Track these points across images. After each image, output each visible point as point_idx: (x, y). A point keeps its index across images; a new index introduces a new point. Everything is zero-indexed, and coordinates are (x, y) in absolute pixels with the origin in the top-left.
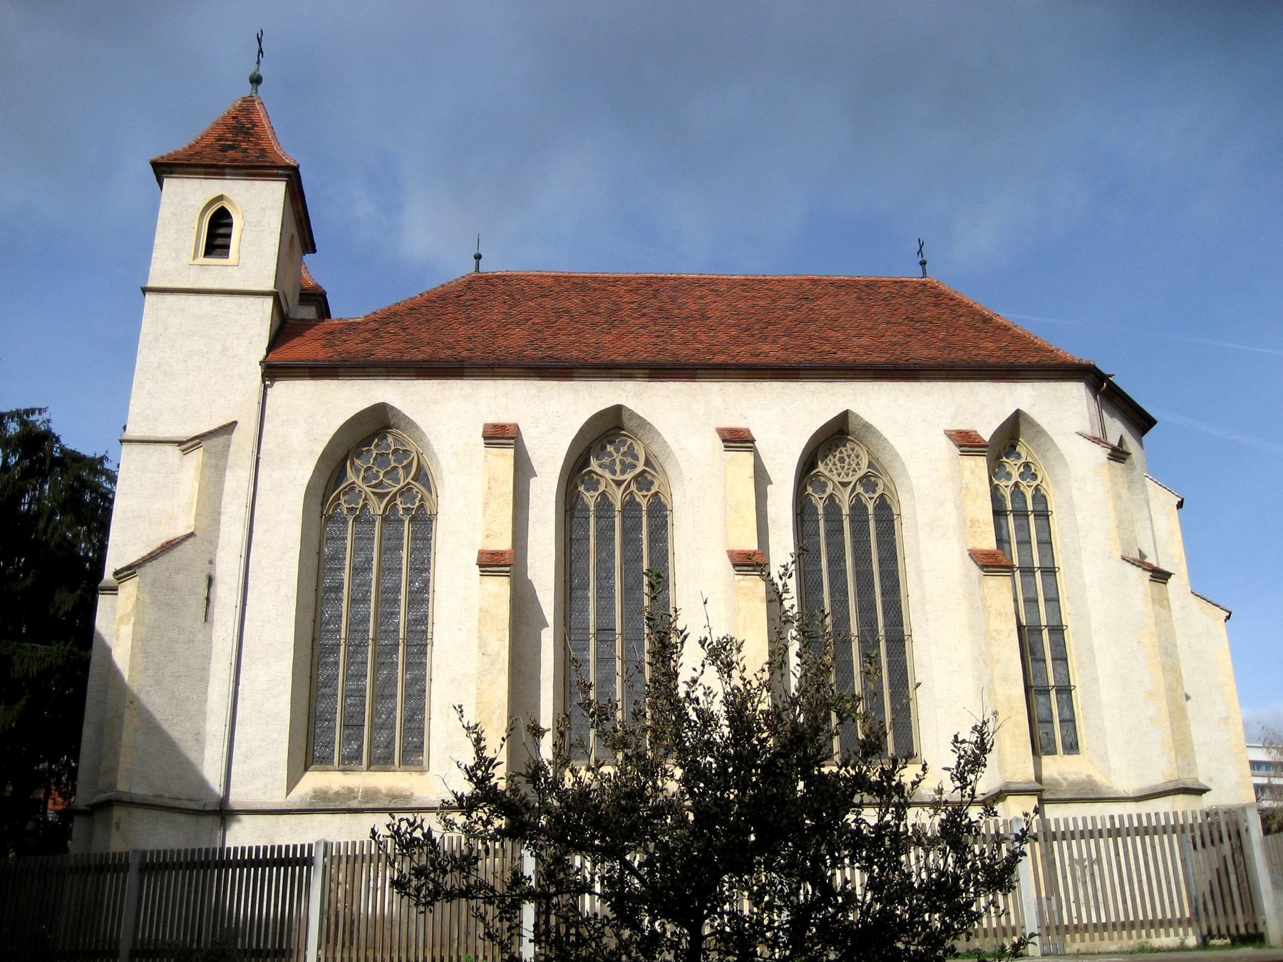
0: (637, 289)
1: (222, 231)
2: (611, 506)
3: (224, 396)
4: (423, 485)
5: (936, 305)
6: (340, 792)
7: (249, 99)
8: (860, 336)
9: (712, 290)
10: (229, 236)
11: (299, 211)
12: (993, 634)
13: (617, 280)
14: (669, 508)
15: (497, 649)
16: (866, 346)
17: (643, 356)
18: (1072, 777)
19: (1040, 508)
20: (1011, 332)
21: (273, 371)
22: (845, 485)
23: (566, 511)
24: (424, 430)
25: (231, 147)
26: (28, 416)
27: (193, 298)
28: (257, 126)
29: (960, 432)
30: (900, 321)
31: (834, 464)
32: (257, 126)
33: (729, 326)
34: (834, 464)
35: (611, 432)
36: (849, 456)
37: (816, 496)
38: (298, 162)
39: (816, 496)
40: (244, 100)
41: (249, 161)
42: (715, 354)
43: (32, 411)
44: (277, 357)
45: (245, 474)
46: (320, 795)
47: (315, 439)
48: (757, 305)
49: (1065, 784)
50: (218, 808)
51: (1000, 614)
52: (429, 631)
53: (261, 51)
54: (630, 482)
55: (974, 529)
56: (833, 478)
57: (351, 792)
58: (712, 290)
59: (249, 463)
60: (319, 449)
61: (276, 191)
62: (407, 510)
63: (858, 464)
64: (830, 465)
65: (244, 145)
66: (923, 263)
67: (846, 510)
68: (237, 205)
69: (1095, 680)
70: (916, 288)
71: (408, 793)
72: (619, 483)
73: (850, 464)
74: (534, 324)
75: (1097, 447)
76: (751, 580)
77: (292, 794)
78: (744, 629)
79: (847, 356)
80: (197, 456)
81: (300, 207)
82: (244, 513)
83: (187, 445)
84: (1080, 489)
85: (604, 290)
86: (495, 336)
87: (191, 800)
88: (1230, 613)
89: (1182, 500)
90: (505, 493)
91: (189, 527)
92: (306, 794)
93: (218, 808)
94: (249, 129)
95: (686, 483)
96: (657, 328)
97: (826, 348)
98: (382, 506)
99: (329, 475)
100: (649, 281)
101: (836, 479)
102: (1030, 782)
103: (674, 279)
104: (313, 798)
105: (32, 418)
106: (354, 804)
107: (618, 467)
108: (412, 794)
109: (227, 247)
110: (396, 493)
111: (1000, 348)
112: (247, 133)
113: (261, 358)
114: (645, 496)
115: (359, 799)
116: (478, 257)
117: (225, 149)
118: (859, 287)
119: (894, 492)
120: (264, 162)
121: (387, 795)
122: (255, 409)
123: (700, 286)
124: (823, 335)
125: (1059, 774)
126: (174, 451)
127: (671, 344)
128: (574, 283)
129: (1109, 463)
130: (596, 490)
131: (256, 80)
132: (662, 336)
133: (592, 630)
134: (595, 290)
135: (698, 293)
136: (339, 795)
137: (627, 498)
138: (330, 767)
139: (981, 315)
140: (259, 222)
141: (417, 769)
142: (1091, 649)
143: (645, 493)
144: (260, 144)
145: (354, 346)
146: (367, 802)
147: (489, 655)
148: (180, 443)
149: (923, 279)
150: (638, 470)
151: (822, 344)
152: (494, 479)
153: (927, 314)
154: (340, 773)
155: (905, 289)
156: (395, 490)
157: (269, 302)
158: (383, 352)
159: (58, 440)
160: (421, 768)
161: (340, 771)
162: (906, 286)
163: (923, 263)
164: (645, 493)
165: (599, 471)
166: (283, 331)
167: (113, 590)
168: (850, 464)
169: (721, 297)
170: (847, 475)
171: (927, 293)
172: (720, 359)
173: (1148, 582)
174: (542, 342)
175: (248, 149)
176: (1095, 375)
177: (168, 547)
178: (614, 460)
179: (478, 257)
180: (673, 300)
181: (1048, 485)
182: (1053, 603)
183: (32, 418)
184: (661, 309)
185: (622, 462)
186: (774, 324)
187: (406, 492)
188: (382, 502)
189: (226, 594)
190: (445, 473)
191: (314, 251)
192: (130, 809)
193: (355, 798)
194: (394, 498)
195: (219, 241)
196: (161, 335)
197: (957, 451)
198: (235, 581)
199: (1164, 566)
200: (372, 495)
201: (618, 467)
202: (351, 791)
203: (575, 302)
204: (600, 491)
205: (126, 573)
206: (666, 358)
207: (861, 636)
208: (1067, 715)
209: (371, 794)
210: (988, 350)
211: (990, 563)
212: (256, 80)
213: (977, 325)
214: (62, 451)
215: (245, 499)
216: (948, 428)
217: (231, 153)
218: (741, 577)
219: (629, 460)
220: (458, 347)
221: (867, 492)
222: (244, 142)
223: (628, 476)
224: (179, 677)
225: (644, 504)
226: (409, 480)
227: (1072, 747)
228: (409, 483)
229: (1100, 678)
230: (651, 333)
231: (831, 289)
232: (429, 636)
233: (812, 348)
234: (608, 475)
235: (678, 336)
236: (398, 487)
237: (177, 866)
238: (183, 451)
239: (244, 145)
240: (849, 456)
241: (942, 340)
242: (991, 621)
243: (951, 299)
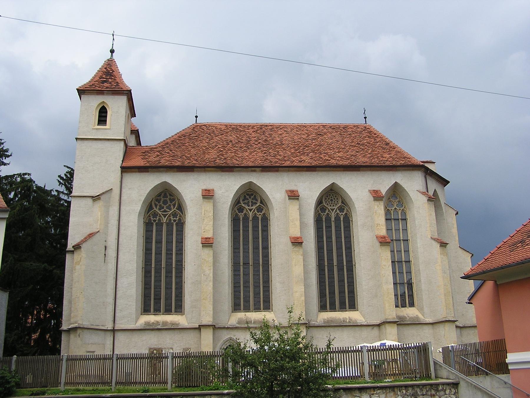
0: (257, 130)
1: (103, 115)
2: (248, 218)
3: (108, 179)
4: (180, 211)
5: (369, 137)
6: (155, 322)
7: (110, 60)
8: (339, 152)
9: (285, 131)
10: (106, 117)
11: (130, 104)
12: (383, 266)
13: (249, 126)
14: (269, 219)
15: (209, 273)
16: (341, 157)
17: (259, 163)
18: (411, 316)
19: (404, 218)
20: (396, 149)
21: (124, 169)
22: (333, 210)
23: (232, 220)
24: (180, 192)
25: (105, 81)
26: (24, 176)
27: (94, 142)
28: (114, 72)
29: (374, 191)
30: (355, 145)
31: (329, 202)
32: (114, 72)
33: (291, 148)
34: (329, 202)
35: (248, 190)
36: (334, 199)
37: (322, 214)
38: (131, 88)
39: (322, 214)
40: (108, 60)
41: (112, 88)
42: (285, 161)
43: (25, 174)
44: (126, 164)
45: (116, 208)
46: (147, 323)
47: (141, 195)
48: (302, 138)
49: (408, 318)
50: (112, 329)
51: (386, 259)
52: (183, 265)
53: (114, 39)
54: (255, 209)
55: (378, 228)
56: (328, 207)
57: (158, 323)
58: (285, 131)
59: (117, 204)
60: (143, 199)
61: (123, 100)
62: (175, 221)
63: (337, 202)
64: (328, 202)
65: (110, 80)
66: (365, 118)
67: (333, 219)
68: (109, 106)
69: (420, 281)
70: (362, 129)
71: (178, 323)
72: (251, 210)
73: (334, 202)
74: (219, 147)
75: (423, 196)
76: (298, 248)
77: (137, 324)
78: (295, 265)
79: (333, 162)
80: (100, 204)
81: (131, 103)
82: (116, 223)
83: (96, 198)
84: (417, 211)
85: (244, 131)
86: (204, 153)
87: (103, 326)
88: (473, 255)
89: (458, 212)
90: (210, 216)
91: (98, 229)
92: (142, 323)
93: (112, 329)
94: (111, 73)
95: (275, 210)
96: (265, 149)
97: (327, 158)
98: (165, 220)
99: (146, 208)
100: (262, 126)
101: (329, 208)
102: (394, 318)
103: (271, 126)
104: (145, 324)
105: (25, 176)
106: (159, 327)
107: (250, 204)
108: (179, 323)
109: (106, 121)
110: (170, 214)
111: (391, 157)
112: (111, 75)
113: (120, 165)
114: (260, 215)
115: (161, 325)
116: (196, 117)
117: (103, 82)
118: (341, 128)
119: (350, 212)
120: (118, 88)
121: (170, 324)
122: (119, 183)
123: (281, 129)
124: (326, 152)
125: (407, 315)
126: (90, 201)
127: (270, 156)
128: (233, 128)
129: (428, 203)
130: (242, 212)
131: (112, 51)
132: (266, 153)
133: (241, 264)
134: (241, 131)
135: (280, 132)
136: (154, 324)
137: (254, 215)
138: (150, 313)
139: (385, 141)
140: (117, 112)
141: (180, 314)
142: (419, 270)
143: (260, 213)
144: (116, 80)
145: (153, 159)
146: (164, 326)
147: (206, 275)
148: (93, 197)
149: (365, 125)
150: (258, 205)
151: (325, 156)
152: (206, 211)
153: (365, 141)
154: (153, 316)
155: (358, 129)
156: (170, 213)
157: (122, 144)
158: (164, 162)
159: (34, 182)
160: (353, 306)
161: (153, 315)
162: (359, 128)
163: (365, 118)
164: (260, 213)
165: (243, 205)
166: (128, 152)
167: (72, 252)
168: (334, 202)
169: (288, 134)
170: (334, 206)
171: (366, 131)
172: (287, 163)
173: (439, 247)
174: (222, 156)
175: (112, 82)
176: (425, 168)
177: (91, 235)
178: (249, 201)
179: (196, 117)
180: (271, 135)
181: (406, 209)
182: (407, 252)
183: (25, 176)
184: (266, 140)
185: (252, 202)
186: (308, 147)
187: (175, 215)
188: (165, 218)
189: (111, 252)
190: (188, 208)
191: (135, 116)
192: (83, 330)
193: (160, 325)
194: (169, 216)
195: (103, 119)
196: (83, 156)
197: (373, 199)
198: (114, 247)
199: (445, 241)
200: (161, 215)
201: (250, 204)
202: (158, 322)
203: (233, 137)
204: (244, 213)
205: (77, 247)
206: (267, 164)
207: (338, 266)
208: (410, 293)
209: (165, 323)
210: (387, 158)
211: (383, 242)
212: (112, 51)
213: (384, 146)
214: (36, 187)
215: (117, 218)
216: (370, 189)
217: (106, 85)
218: (294, 247)
219: (254, 201)
220: (192, 159)
221: (340, 212)
222: (110, 79)
223: (254, 207)
224: (97, 283)
225: (260, 217)
226: (175, 209)
227: (412, 305)
228: (175, 210)
229: (422, 281)
230: (262, 151)
231: (330, 130)
232: (183, 266)
233: (321, 158)
234: (247, 207)
235: (272, 153)
236: (171, 212)
237: (128, 358)
238: (93, 200)
239: (110, 80)
240: (334, 199)
241: (370, 154)
242: (382, 262)
243: (375, 134)
